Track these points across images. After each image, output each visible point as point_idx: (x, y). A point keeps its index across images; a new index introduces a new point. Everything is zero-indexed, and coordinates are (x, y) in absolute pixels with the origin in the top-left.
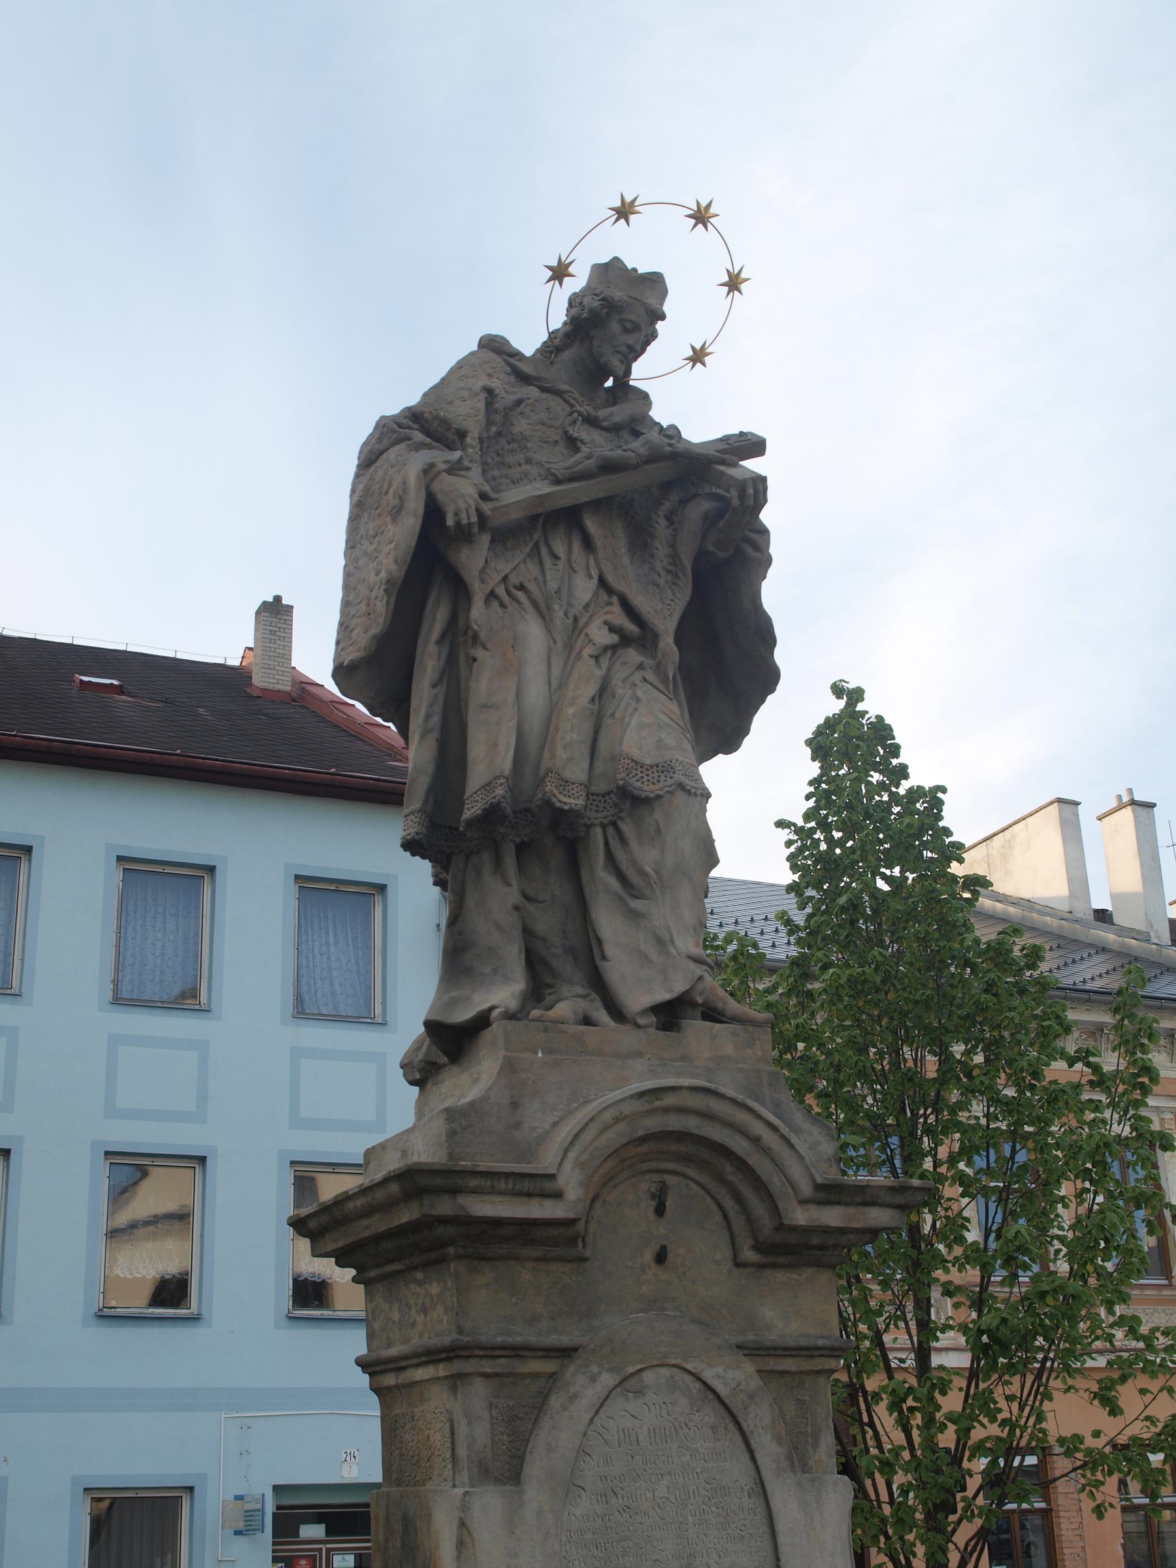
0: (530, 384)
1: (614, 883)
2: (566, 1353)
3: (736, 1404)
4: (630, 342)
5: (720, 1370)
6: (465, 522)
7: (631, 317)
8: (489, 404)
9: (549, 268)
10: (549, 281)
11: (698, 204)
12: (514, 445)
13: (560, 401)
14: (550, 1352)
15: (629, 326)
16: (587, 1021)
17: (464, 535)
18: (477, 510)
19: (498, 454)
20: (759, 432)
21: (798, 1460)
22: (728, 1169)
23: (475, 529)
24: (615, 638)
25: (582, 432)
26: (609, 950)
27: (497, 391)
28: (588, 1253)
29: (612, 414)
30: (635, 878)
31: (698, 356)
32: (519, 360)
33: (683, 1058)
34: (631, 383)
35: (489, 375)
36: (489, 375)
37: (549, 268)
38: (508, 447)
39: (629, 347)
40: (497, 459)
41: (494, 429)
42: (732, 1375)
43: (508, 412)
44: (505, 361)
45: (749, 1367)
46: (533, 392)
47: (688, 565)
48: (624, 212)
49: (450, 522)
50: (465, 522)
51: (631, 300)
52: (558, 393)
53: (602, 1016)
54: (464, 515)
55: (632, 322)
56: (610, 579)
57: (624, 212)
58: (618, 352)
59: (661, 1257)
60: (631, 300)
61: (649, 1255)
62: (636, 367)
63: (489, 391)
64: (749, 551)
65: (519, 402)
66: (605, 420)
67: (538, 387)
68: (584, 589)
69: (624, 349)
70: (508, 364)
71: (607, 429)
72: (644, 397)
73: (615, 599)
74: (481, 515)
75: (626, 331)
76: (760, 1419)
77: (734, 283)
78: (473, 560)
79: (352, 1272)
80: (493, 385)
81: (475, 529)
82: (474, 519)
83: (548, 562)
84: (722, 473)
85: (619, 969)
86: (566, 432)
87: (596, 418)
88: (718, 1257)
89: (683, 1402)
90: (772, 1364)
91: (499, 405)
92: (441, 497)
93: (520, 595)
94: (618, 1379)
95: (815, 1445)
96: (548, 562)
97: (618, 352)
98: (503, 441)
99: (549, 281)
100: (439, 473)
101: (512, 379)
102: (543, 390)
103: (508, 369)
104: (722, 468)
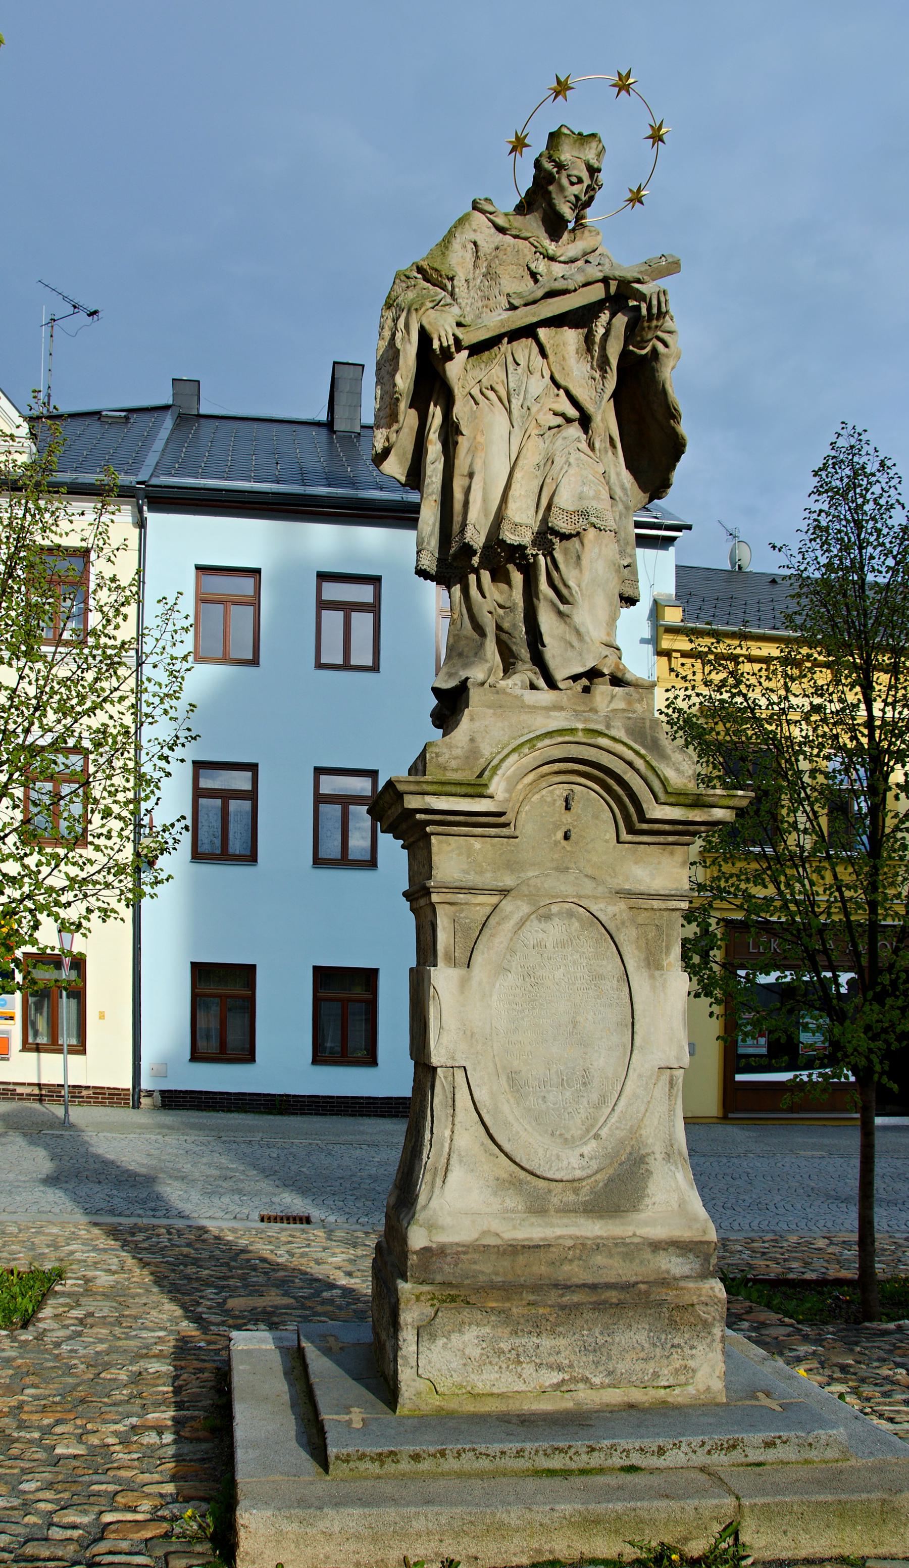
1: (551, 593)
2: (504, 892)
3: (611, 927)
5: (602, 906)
7: (575, 172)
14: (492, 891)
15: (574, 180)
16: (533, 687)
17: (447, 355)
21: (653, 963)
22: (611, 782)
23: (453, 349)
24: (559, 420)
25: (541, 266)
26: (547, 639)
28: (517, 833)
30: (564, 591)
31: (636, 198)
33: (591, 710)
42: (611, 911)
45: (622, 905)
46: (508, 239)
47: (614, 362)
48: (561, 88)
49: (436, 345)
53: (541, 683)
54: (444, 340)
56: (557, 377)
57: (561, 88)
59: (567, 837)
61: (560, 835)
68: (538, 385)
70: (490, 220)
71: (565, 263)
73: (562, 392)
74: (457, 340)
75: (572, 184)
76: (627, 937)
77: (656, 137)
78: (456, 369)
79: (401, 842)
81: (453, 349)
82: (451, 342)
83: (511, 366)
85: (552, 651)
88: (607, 837)
89: (576, 924)
90: (633, 902)
92: (427, 327)
93: (490, 394)
94: (534, 909)
95: (668, 952)
96: (511, 366)
104: (636, 285)
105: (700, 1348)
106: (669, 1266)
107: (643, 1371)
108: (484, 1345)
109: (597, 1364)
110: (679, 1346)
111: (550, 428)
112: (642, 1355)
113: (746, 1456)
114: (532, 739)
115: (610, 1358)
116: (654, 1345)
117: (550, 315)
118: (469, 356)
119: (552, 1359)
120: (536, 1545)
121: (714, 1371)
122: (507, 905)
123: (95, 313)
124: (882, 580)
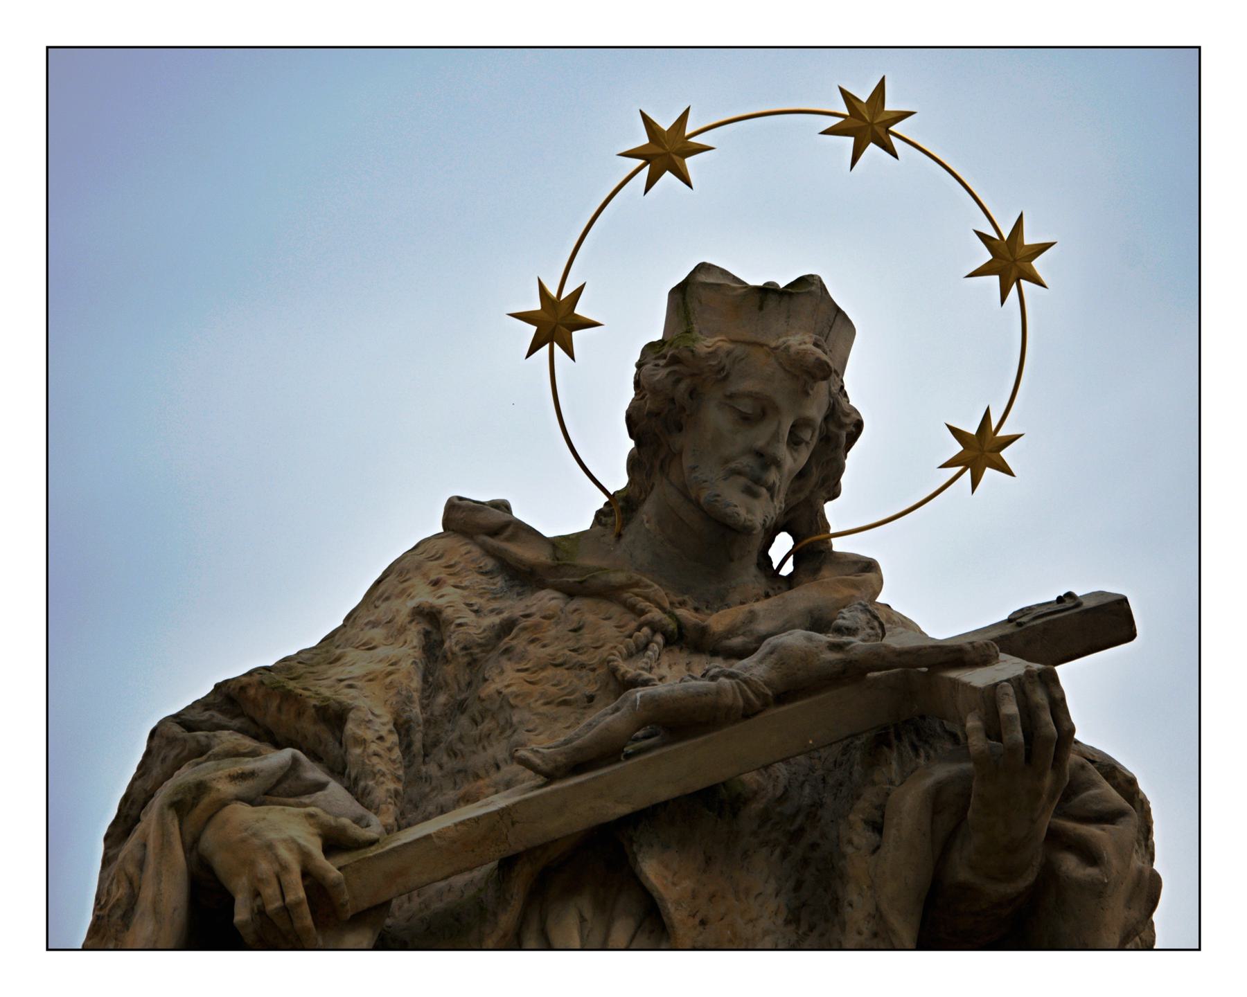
0: (542, 586)
4: (760, 443)
6: (274, 905)
8: (432, 649)
9: (1004, 468)
10: (534, 348)
11: (847, 97)
12: (487, 725)
13: (615, 610)
15: (746, 406)
18: (305, 874)
19: (453, 753)
20: (1114, 588)
27: (448, 612)
29: (752, 616)
32: (512, 539)
34: (838, 545)
35: (436, 583)
36: (436, 583)
37: (1004, 468)
38: (475, 732)
39: (759, 454)
40: (450, 764)
41: (442, 699)
43: (475, 659)
44: (483, 546)
50: (274, 905)
51: (739, 350)
52: (608, 593)
54: (271, 891)
55: (750, 395)
57: (666, 152)
58: (738, 473)
60: (739, 350)
62: (835, 513)
63: (431, 617)
64: (1071, 865)
65: (507, 627)
66: (731, 632)
67: (556, 588)
69: (747, 462)
72: (866, 570)
80: (438, 602)
82: (297, 892)
84: (955, 683)
86: (613, 671)
87: (703, 630)
91: (451, 643)
92: (222, 862)
97: (738, 473)
98: (464, 720)
99: (534, 348)
100: (223, 804)
101: (499, 582)
102: (571, 593)
103: (489, 563)
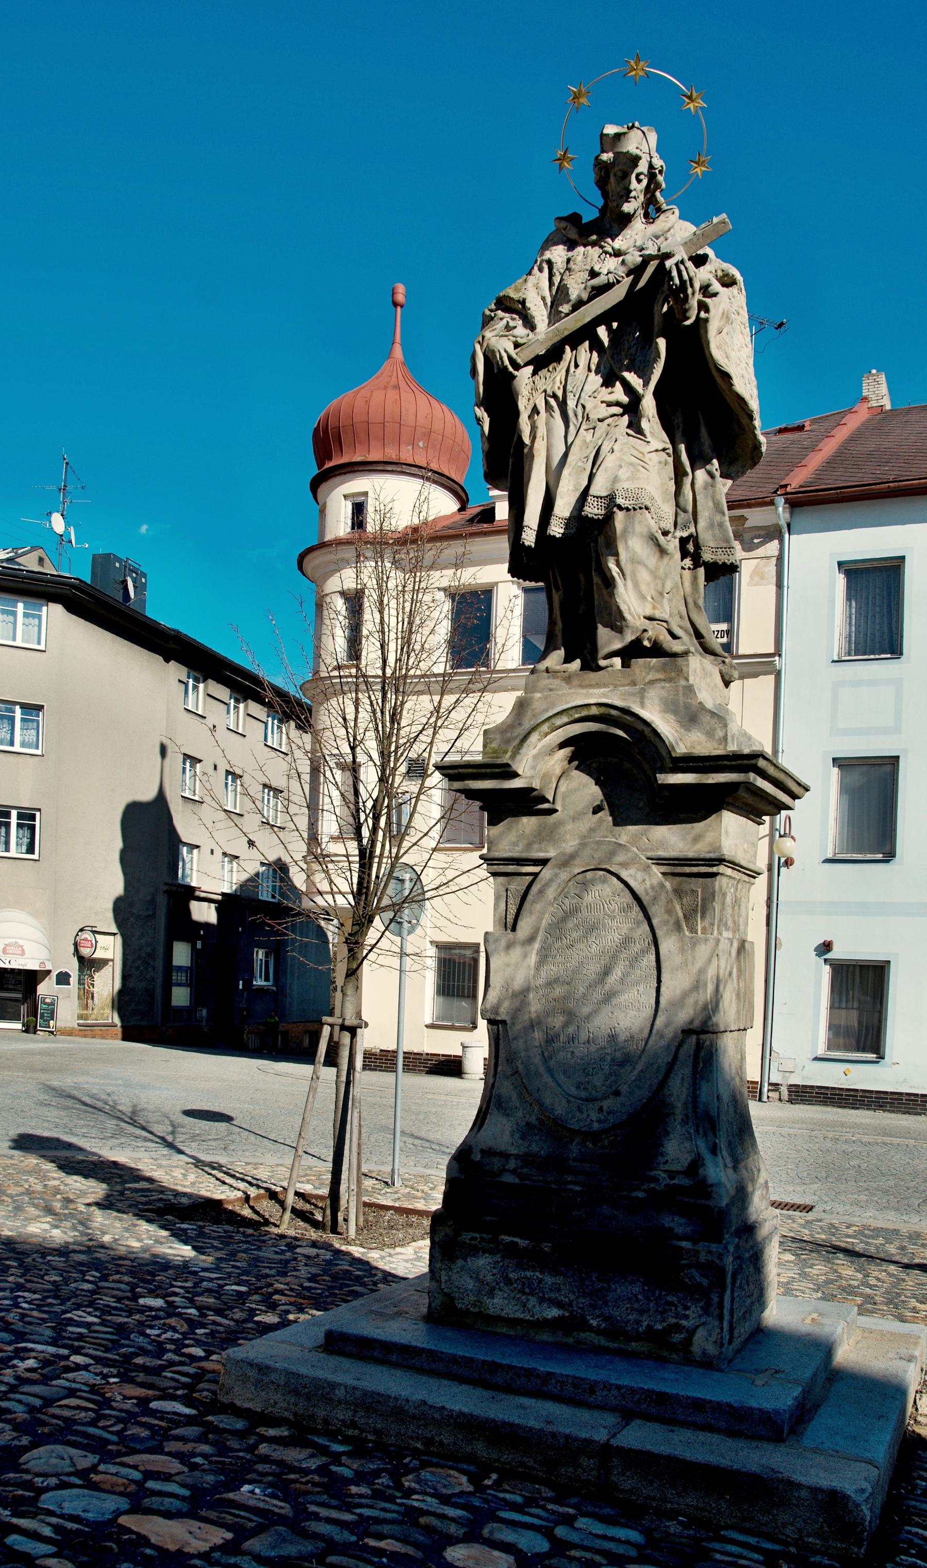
105: (693, 1308)
106: (671, 1225)
107: (637, 1322)
108: (494, 1271)
109: (594, 1306)
110: (672, 1304)
111: (600, 420)
112: (636, 1306)
113: (675, 1413)
114: (551, 717)
115: (606, 1303)
116: (649, 1300)
117: (599, 312)
118: (535, 373)
119: (553, 1295)
120: (429, 1435)
121: (710, 1335)
122: (546, 873)
123: (781, 325)
124: (367, 564)
